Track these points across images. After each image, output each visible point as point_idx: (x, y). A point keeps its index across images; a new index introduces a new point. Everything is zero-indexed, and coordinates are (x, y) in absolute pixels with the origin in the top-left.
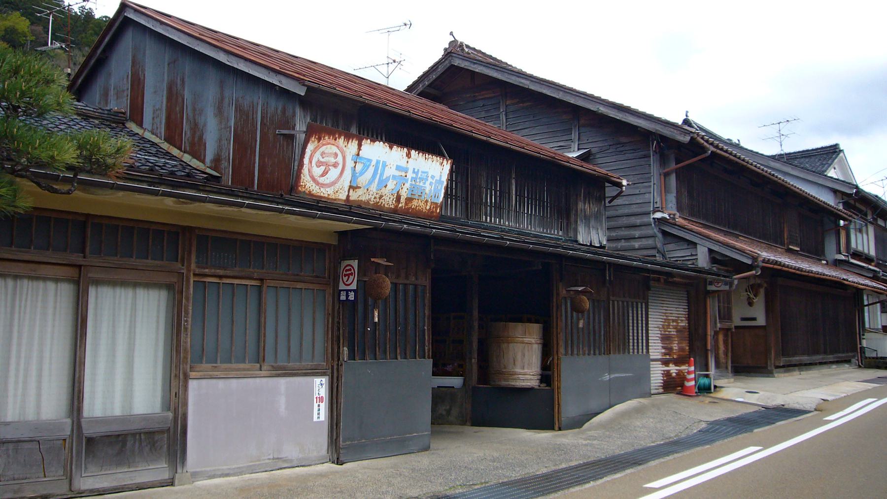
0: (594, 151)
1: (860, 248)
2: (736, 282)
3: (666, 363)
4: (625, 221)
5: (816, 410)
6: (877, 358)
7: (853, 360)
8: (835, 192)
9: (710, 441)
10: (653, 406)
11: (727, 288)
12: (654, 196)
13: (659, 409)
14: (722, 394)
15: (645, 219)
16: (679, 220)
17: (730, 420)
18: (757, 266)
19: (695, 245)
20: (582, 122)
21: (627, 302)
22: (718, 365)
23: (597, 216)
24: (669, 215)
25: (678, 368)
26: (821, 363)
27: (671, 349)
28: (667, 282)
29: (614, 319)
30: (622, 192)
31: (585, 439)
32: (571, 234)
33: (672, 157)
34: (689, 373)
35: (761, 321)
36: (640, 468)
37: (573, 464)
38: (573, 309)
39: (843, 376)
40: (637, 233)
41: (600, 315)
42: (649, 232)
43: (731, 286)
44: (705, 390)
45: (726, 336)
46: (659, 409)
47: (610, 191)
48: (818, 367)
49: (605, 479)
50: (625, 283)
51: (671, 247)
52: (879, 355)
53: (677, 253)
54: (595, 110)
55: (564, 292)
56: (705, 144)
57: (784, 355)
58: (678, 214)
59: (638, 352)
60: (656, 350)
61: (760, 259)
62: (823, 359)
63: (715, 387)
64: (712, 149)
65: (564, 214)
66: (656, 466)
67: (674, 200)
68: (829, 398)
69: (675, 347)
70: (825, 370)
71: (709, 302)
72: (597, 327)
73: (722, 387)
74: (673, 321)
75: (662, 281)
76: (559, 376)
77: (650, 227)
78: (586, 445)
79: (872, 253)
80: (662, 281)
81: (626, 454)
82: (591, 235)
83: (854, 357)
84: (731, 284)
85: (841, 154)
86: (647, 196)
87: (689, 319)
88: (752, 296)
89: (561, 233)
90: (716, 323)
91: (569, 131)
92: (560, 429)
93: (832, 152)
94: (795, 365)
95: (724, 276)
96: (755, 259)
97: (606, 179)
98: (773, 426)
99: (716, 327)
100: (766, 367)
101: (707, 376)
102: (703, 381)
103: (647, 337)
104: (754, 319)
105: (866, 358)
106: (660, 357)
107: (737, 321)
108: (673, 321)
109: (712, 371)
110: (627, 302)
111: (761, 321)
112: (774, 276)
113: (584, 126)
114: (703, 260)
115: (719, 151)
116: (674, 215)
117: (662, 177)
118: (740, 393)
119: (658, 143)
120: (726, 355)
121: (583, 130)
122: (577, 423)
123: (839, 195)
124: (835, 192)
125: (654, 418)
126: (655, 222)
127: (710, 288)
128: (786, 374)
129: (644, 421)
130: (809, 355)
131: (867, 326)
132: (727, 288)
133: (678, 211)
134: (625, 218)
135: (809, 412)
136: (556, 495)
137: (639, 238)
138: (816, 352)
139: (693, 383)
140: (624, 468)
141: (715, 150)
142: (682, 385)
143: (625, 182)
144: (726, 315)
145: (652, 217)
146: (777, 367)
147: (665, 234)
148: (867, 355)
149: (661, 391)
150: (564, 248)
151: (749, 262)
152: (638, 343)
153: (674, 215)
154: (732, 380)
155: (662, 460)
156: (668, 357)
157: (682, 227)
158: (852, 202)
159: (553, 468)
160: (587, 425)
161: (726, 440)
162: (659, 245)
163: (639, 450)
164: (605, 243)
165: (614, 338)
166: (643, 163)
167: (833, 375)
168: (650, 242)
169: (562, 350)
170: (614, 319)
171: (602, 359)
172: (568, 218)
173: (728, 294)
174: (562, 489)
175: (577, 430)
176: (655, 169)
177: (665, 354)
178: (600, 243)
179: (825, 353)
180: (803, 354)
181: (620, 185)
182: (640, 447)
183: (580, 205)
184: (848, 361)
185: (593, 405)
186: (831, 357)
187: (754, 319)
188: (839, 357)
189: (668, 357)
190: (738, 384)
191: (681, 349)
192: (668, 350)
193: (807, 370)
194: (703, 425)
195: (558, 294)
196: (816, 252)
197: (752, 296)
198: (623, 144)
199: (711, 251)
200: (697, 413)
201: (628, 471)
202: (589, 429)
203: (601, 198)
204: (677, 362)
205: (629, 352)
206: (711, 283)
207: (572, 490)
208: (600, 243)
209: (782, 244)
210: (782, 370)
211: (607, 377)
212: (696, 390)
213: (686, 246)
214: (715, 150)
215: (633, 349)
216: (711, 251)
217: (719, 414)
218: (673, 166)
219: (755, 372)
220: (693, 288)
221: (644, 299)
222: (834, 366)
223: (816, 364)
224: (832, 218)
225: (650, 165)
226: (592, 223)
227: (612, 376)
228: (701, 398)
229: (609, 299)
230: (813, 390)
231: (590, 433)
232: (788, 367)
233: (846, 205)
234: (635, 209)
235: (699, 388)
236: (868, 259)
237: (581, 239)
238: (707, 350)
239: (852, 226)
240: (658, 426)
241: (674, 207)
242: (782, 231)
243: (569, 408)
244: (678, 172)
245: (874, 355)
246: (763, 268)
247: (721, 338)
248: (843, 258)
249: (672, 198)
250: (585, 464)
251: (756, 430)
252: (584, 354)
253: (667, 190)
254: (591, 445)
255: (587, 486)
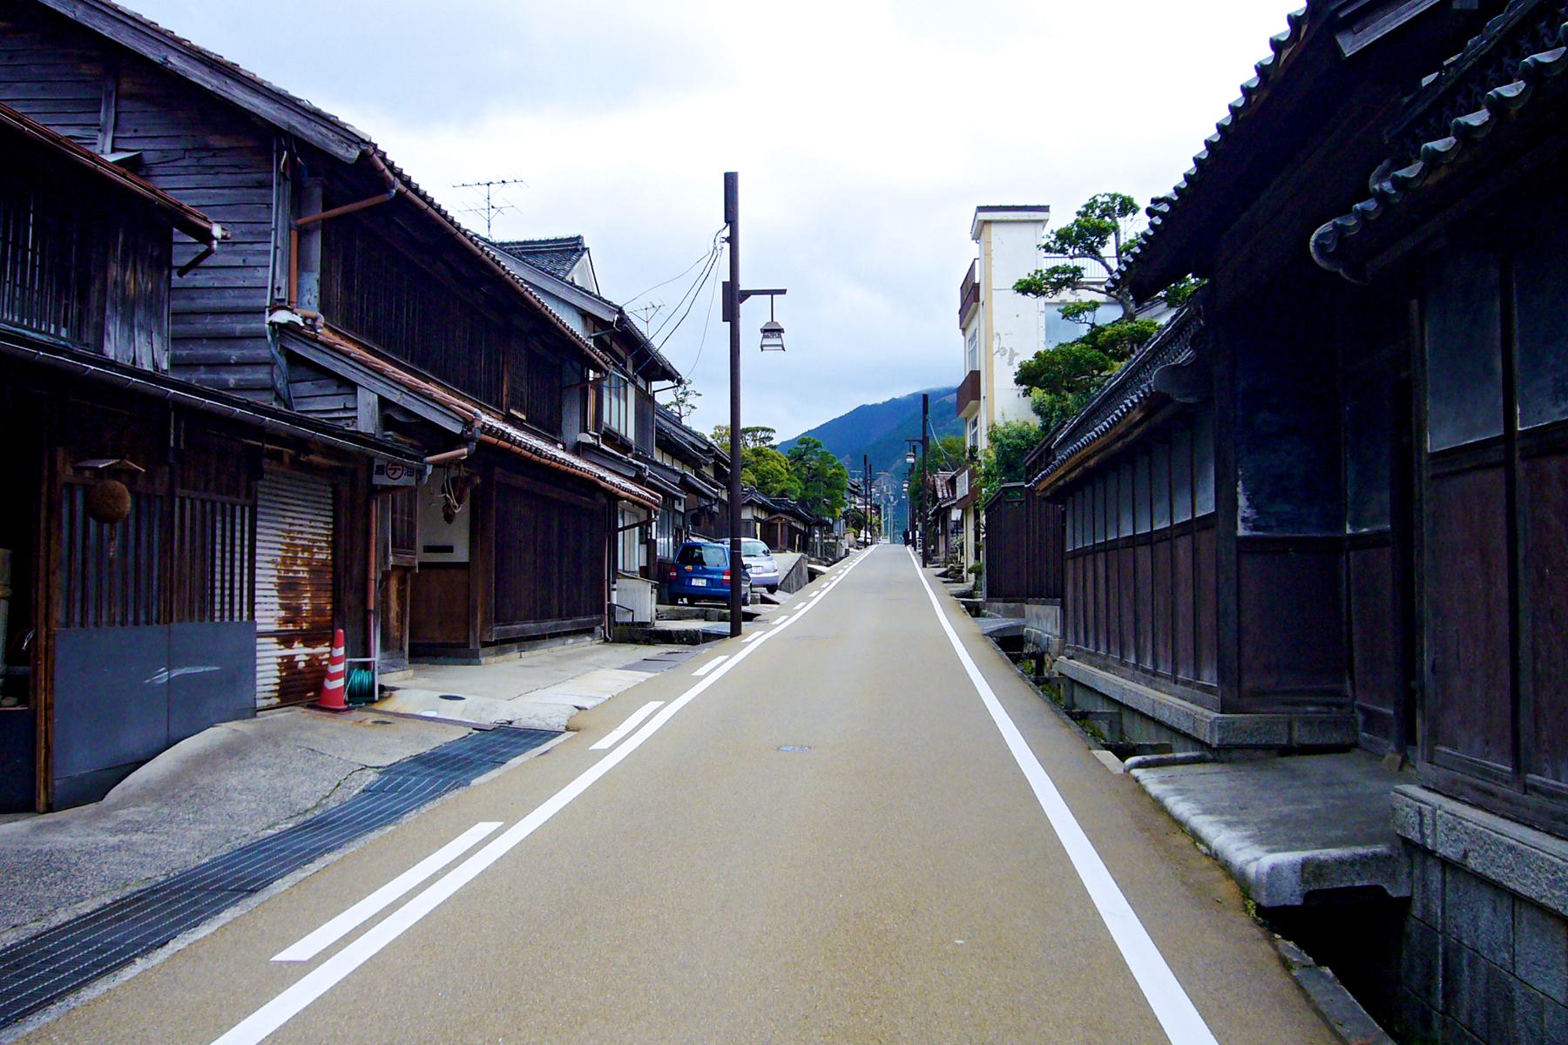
0: (149, 157)
1: (614, 426)
2: (429, 470)
3: (286, 640)
4: (209, 324)
5: (567, 729)
6: (633, 624)
7: (598, 629)
8: (585, 316)
9: (393, 816)
10: (264, 737)
11: (412, 481)
12: (271, 271)
13: (277, 745)
14: (393, 705)
15: (253, 325)
16: (324, 334)
17: (419, 760)
18: (472, 439)
19: (352, 387)
20: (126, 86)
21: (213, 503)
22: (385, 646)
23: (153, 304)
24: (305, 319)
25: (309, 650)
26: (553, 636)
27: (298, 609)
28: (295, 463)
29: (182, 542)
30: (209, 252)
31: (114, 832)
32: (89, 337)
33: (318, 193)
34: (334, 660)
35: (461, 554)
36: (254, 901)
37: (88, 907)
38: (90, 510)
39: (590, 659)
40: (234, 354)
41: (151, 529)
42: (263, 351)
43: (419, 479)
44: (363, 697)
45: (402, 581)
46: (277, 745)
47: (184, 249)
48: (548, 643)
49: (174, 946)
50: (218, 455)
51: (305, 388)
52: (637, 620)
53: (319, 403)
54: (157, 59)
55: (70, 471)
56: (387, 172)
57: (498, 620)
58: (322, 319)
59: (232, 617)
60: (269, 614)
61: (478, 424)
62: (556, 626)
63: (382, 688)
64: (399, 186)
65: (75, 287)
66: (288, 892)
67: (315, 288)
68: (588, 704)
69: (306, 605)
70: (571, 645)
71: (375, 509)
72: (143, 559)
73: (394, 689)
74: (305, 548)
75: (286, 459)
76: (50, 677)
77: (261, 343)
78: (116, 848)
79: (631, 436)
80: (286, 459)
81: (214, 864)
82: (135, 348)
83: (599, 622)
84: (422, 472)
85: (586, 255)
86: (260, 273)
87: (334, 546)
88: (453, 502)
89: (64, 333)
90: (386, 556)
91: (94, 105)
92: (50, 808)
93: (572, 248)
94: (512, 641)
95: (409, 457)
96: (468, 423)
97: (178, 218)
98: (504, 768)
99: (386, 563)
100: (466, 645)
101: (366, 666)
102: (360, 677)
103: (252, 582)
104: (449, 549)
105: (616, 624)
106: (275, 627)
107: (421, 557)
108: (305, 548)
109: (377, 657)
110: (213, 503)
111: (461, 554)
112: (494, 457)
113: (131, 97)
114: (366, 419)
115: (409, 193)
116: (315, 319)
117: (294, 233)
118: (436, 701)
119: (291, 158)
120: (401, 621)
121: (126, 105)
122: (93, 790)
123: (590, 322)
124: (585, 316)
125: (267, 767)
126: (273, 333)
127: (379, 480)
128: (500, 658)
129: (247, 775)
130: (536, 620)
131: (620, 567)
132: (412, 481)
133: (322, 312)
134: (209, 319)
135: (557, 734)
136: (45, 1019)
137: (237, 364)
138: (546, 615)
139: (340, 683)
140: (216, 909)
141: (404, 189)
142: (319, 688)
143: (217, 231)
144: (404, 542)
145: (268, 319)
146: (486, 644)
147: (294, 360)
148: (619, 618)
149: (275, 701)
150: (73, 356)
151: (457, 429)
152: (232, 596)
153: (315, 319)
154: (410, 673)
155: (299, 875)
156: (291, 627)
157: (331, 347)
158: (607, 339)
159: (35, 927)
160: (114, 795)
161: (423, 810)
162: (280, 384)
163: (245, 850)
164: (165, 366)
165: (183, 588)
166: (256, 199)
167: (571, 657)
168: (261, 375)
169: (59, 614)
170: (182, 542)
171: (153, 634)
172: (84, 298)
173: (411, 492)
174: (61, 996)
175: (91, 808)
176: (278, 216)
177: (285, 621)
178: (156, 366)
179: (560, 616)
180: (527, 618)
181: (206, 237)
182: (245, 842)
183: (114, 271)
184: (589, 631)
185: (132, 742)
186: (567, 625)
187: (449, 549)
188: (579, 624)
189: (291, 627)
190: (422, 681)
191: (317, 610)
192: (293, 613)
193: (531, 648)
194: (371, 777)
195: (53, 475)
196: (551, 429)
197: (453, 502)
198: (216, 152)
199: (384, 403)
200: (353, 751)
201: (227, 915)
202: (122, 804)
203: (162, 264)
204: (309, 639)
205: (212, 618)
206: (381, 470)
207: (87, 994)
208: (156, 366)
209: (499, 405)
210: (493, 649)
211: (163, 676)
212: (346, 696)
213: (334, 390)
214: (404, 189)
215: (222, 610)
216: (384, 403)
217: (398, 748)
218: (317, 214)
219: (448, 655)
220: (345, 478)
221: (248, 496)
222: (571, 641)
223: (543, 637)
224: (577, 365)
225: (269, 206)
226: (139, 316)
227: (176, 673)
228: (356, 715)
229: (171, 495)
230: (554, 689)
231: (124, 814)
232: (503, 644)
233: (598, 341)
234: (230, 300)
235: (352, 694)
236: (624, 446)
237: (110, 351)
238: (367, 612)
239: (606, 383)
240: (278, 783)
241: (315, 303)
242: (500, 380)
243: (77, 761)
244: (327, 226)
245: (628, 618)
246: (482, 443)
247: (394, 585)
248: (590, 440)
249: (312, 281)
250: (119, 905)
251: (475, 782)
252: (112, 623)
253: (303, 266)
254: (130, 847)
255: (129, 973)
